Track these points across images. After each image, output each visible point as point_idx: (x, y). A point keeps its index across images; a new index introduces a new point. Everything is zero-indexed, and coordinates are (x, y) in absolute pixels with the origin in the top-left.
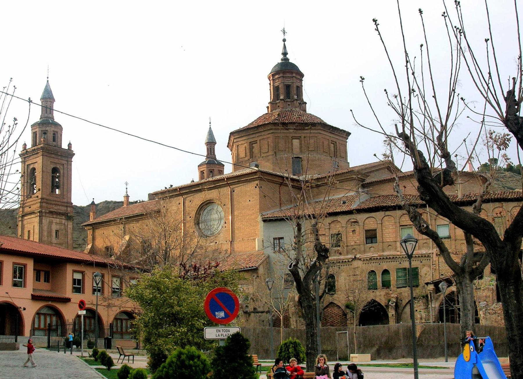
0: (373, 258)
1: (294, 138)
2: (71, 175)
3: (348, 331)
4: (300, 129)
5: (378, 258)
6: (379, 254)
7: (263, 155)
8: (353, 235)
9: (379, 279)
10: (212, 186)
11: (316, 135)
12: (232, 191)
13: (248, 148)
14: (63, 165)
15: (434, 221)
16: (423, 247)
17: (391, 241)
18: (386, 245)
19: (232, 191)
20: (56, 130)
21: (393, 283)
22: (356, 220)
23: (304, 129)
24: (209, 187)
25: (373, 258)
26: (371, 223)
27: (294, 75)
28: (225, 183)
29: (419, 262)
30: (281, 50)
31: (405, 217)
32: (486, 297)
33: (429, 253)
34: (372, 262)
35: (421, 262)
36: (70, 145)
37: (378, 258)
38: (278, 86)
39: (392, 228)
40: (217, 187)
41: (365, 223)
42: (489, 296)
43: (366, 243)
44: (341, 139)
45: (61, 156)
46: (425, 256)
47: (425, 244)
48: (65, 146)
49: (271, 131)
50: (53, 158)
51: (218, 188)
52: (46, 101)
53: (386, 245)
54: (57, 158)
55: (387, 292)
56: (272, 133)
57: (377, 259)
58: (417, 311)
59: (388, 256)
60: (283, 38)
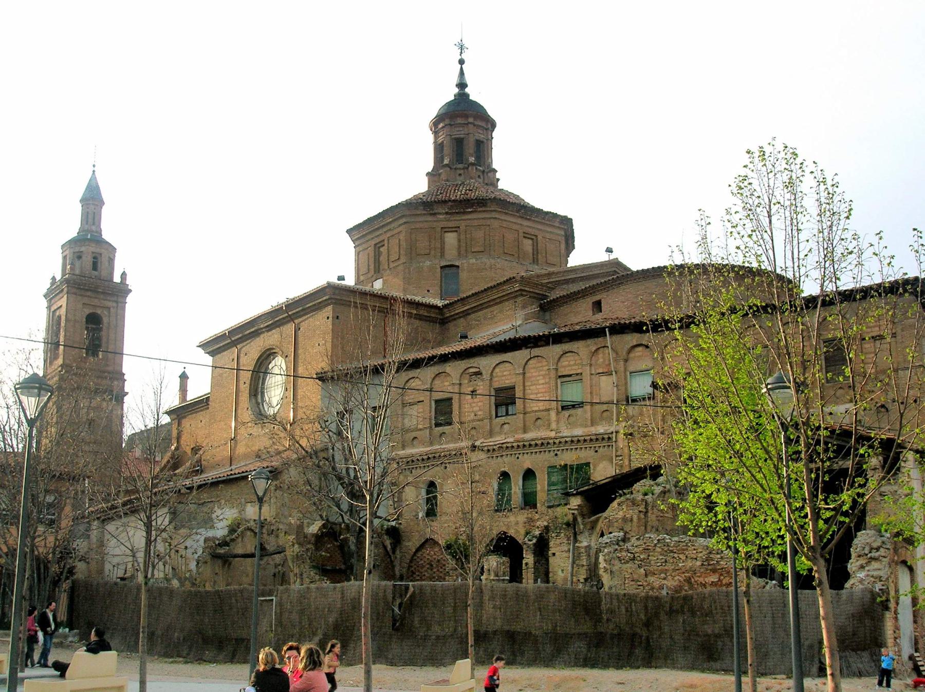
0: (504, 446)
1: (445, 230)
2: (124, 326)
3: (276, 596)
4: (457, 213)
5: (514, 444)
6: (516, 436)
7: (392, 265)
8: (471, 401)
9: (516, 488)
10: (270, 322)
11: (488, 222)
12: (297, 329)
13: (372, 254)
14: (109, 308)
15: (622, 363)
16: (602, 419)
17: (541, 408)
18: (530, 418)
19: (297, 329)
20: (98, 250)
21: (541, 497)
22: (478, 370)
23: (464, 213)
24: (266, 324)
25: (504, 446)
26: (505, 373)
27: (471, 120)
28: (284, 316)
29: (592, 452)
30: (455, 79)
31: (569, 359)
32: (625, 519)
33: (609, 431)
34: (504, 454)
35: (596, 451)
36: (124, 275)
37: (515, 444)
38: (443, 142)
39: (543, 381)
40: (278, 323)
41: (494, 374)
42: (632, 520)
43: (497, 416)
44: (549, 229)
45: (103, 293)
46: (603, 439)
47: (605, 414)
48: (117, 279)
49: (404, 220)
50: (89, 296)
51: (279, 326)
52: (87, 204)
53: (530, 418)
54: (96, 298)
55: (530, 516)
56: (405, 223)
57: (513, 447)
58: (554, 554)
59: (532, 440)
60: (460, 57)
